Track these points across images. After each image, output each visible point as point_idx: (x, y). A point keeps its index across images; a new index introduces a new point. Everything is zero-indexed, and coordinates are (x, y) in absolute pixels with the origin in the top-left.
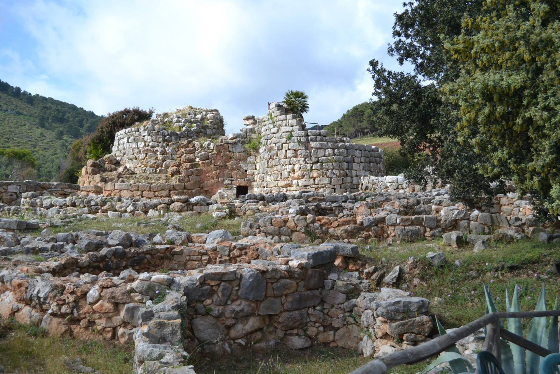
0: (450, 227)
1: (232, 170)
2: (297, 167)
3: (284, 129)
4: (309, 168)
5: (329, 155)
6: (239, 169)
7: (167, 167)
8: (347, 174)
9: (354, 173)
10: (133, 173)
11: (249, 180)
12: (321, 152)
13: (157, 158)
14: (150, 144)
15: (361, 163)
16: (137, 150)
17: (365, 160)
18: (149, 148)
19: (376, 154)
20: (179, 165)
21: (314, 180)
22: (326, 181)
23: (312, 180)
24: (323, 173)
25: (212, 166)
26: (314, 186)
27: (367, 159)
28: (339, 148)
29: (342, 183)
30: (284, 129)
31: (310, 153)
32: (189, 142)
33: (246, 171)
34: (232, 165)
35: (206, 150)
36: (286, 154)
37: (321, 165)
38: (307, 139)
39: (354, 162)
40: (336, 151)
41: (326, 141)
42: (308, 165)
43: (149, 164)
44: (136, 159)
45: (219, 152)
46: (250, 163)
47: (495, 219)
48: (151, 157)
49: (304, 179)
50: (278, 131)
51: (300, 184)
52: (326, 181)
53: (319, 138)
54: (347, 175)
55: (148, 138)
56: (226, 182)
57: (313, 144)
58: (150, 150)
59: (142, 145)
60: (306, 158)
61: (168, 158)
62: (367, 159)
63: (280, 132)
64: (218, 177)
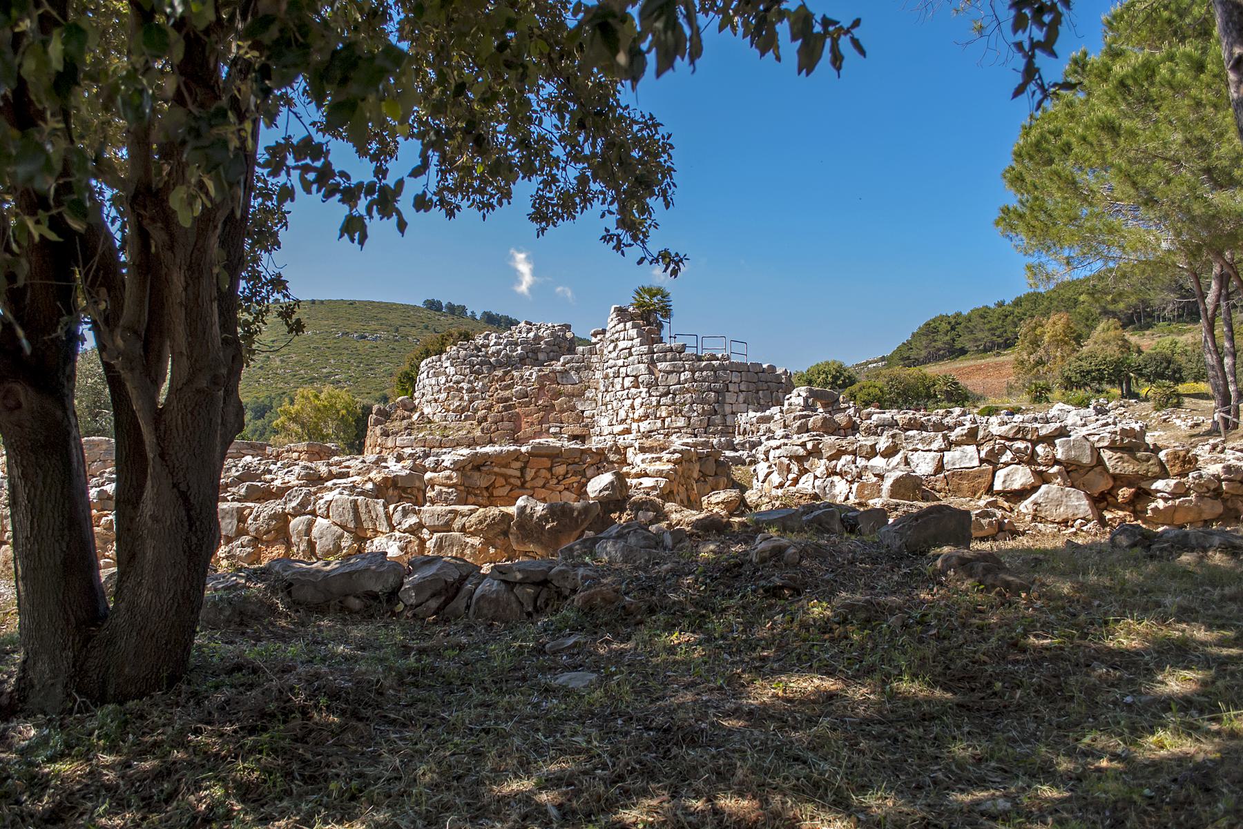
0: (268, 532)
1: (562, 411)
2: (638, 402)
3: (621, 345)
4: (655, 403)
5: (686, 381)
6: (573, 409)
7: (476, 410)
8: (715, 411)
9: (728, 409)
10: (430, 422)
11: (586, 426)
12: (673, 379)
13: (462, 399)
14: (454, 378)
15: (741, 391)
16: (436, 388)
17: (748, 387)
18: (451, 384)
19: (769, 377)
20: (489, 408)
21: (663, 421)
22: (681, 422)
23: (659, 422)
24: (675, 410)
25: (532, 407)
26: (662, 431)
27: (752, 387)
28: (702, 370)
29: (708, 425)
30: (621, 345)
31: (657, 379)
32: (506, 373)
33: (583, 412)
34: (561, 405)
35: (525, 383)
36: (623, 384)
37: (673, 399)
38: (652, 357)
39: (728, 391)
40: (697, 374)
41: (681, 359)
42: (654, 399)
43: (452, 407)
44: (436, 401)
45: (542, 387)
46: (588, 399)
47: (362, 510)
48: (454, 397)
49: (648, 421)
50: (614, 350)
51: (642, 430)
52: (681, 422)
53: (669, 355)
54: (716, 412)
55: (451, 370)
56: (552, 430)
57: (661, 366)
58: (453, 387)
59: (442, 379)
60: (649, 388)
61: (477, 398)
62: (752, 387)
63: (617, 350)
64: (541, 423)
